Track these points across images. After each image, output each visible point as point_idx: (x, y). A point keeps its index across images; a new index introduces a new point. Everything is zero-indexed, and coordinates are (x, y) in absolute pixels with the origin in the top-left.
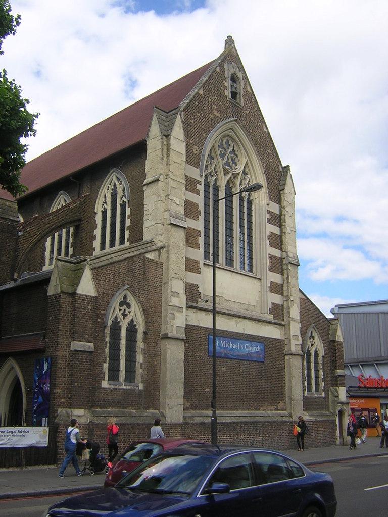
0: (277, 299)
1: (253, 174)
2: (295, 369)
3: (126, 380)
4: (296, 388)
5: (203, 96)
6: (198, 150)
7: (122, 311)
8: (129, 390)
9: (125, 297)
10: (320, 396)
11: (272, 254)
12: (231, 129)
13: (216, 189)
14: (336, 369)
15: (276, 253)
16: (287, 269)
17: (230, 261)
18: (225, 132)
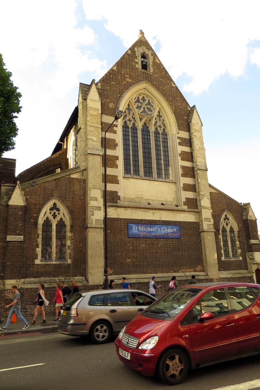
0: (190, 195)
2: (209, 240)
4: (211, 256)
5: (117, 71)
6: (113, 105)
8: (58, 264)
9: (226, 215)
10: (238, 259)
11: (183, 165)
12: (145, 89)
13: (134, 128)
14: (250, 240)
16: (197, 173)
17: (137, 172)
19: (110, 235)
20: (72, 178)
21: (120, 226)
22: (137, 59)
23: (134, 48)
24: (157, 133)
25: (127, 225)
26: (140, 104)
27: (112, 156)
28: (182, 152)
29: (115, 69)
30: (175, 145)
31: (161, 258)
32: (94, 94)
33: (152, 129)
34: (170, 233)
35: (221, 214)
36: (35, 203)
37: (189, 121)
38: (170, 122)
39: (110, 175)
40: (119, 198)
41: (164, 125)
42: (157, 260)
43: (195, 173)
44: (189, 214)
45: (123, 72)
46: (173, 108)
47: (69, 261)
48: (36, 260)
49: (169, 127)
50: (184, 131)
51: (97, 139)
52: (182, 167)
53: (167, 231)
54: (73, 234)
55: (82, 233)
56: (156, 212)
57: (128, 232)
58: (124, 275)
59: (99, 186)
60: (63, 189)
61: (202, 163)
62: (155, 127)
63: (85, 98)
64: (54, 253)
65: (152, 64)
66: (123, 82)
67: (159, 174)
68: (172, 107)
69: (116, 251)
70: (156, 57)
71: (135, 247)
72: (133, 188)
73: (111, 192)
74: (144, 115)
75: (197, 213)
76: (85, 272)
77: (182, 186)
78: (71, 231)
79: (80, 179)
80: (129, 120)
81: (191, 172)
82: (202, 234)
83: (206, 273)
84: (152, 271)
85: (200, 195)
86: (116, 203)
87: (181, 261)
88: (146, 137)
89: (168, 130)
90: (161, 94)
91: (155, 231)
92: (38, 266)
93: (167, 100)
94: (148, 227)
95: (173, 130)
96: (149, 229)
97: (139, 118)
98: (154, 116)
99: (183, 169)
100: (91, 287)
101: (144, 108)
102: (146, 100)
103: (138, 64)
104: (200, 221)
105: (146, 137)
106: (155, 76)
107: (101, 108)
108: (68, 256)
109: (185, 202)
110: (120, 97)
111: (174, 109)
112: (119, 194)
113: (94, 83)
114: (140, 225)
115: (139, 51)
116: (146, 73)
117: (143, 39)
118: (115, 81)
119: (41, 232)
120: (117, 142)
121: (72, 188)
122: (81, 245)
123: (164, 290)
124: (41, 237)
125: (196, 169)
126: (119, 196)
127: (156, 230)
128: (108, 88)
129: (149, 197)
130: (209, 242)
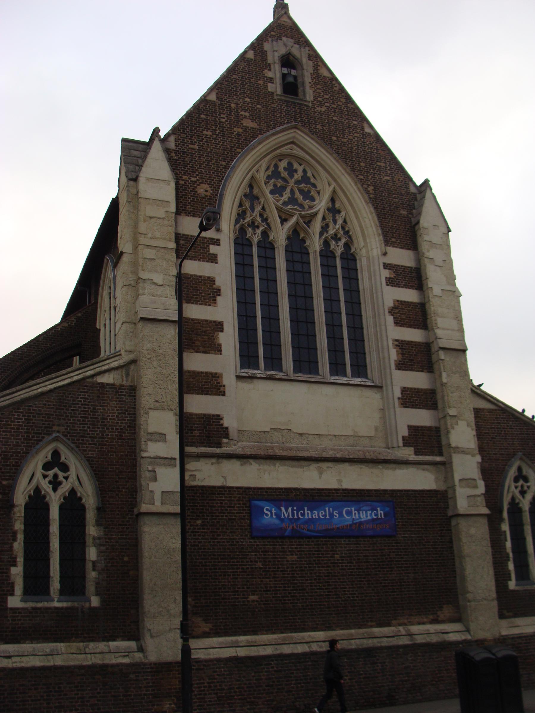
0: (423, 418)
1: (349, 208)
3: (62, 592)
6: (209, 189)
7: (519, 488)
8: (67, 608)
9: (520, 469)
13: (267, 246)
15: (414, 335)
17: (274, 361)
18: (278, 151)
19: (202, 532)
20: (99, 383)
21: (228, 507)
22: (270, 70)
23: (262, 44)
24: (327, 254)
25: (248, 505)
28: (396, 303)
29: (213, 97)
31: (341, 588)
32: (157, 166)
33: (315, 245)
34: (367, 522)
35: (507, 467)
36: (5, 452)
37: (414, 221)
38: (363, 224)
39: (202, 373)
40: (225, 432)
41: (347, 233)
42: (330, 595)
43: (434, 358)
44: (418, 468)
45: (233, 106)
46: (369, 189)
47: (95, 601)
48: (10, 598)
51: (164, 279)
52: (397, 343)
53: (357, 517)
54: (105, 531)
55: (128, 528)
56: (328, 467)
57: (251, 523)
58: (240, 635)
59: (169, 403)
60: (77, 412)
61: (453, 330)
62: (322, 241)
63: (134, 177)
64: (54, 579)
65: (310, 81)
66: (235, 129)
67: (337, 367)
68: (366, 186)
69: (218, 572)
70: (320, 63)
71: (270, 562)
72: (264, 406)
75: (439, 466)
76: (138, 629)
77: (398, 393)
78: (98, 523)
79: (122, 386)
81: (419, 356)
82: (453, 522)
83: (465, 626)
84: (317, 624)
85: (448, 418)
87: (397, 595)
88: (298, 267)
89: (359, 243)
90: (335, 155)
91: (325, 518)
92: (15, 613)
93: (353, 169)
94: (306, 508)
96: (308, 514)
98: (319, 211)
100: (151, 668)
103: (273, 83)
104: (448, 488)
105: (298, 267)
106: (319, 109)
108: (91, 587)
109: (406, 437)
111: (371, 192)
114: (283, 503)
115: (275, 51)
116: (294, 103)
117: (284, 21)
118: (214, 128)
119: (22, 527)
120: (218, 283)
121: (99, 409)
122: (126, 559)
123: (349, 672)
124: (23, 539)
125: (434, 348)
126: (227, 428)
127: (328, 517)
128: (196, 147)
129: (308, 424)
130: (474, 542)
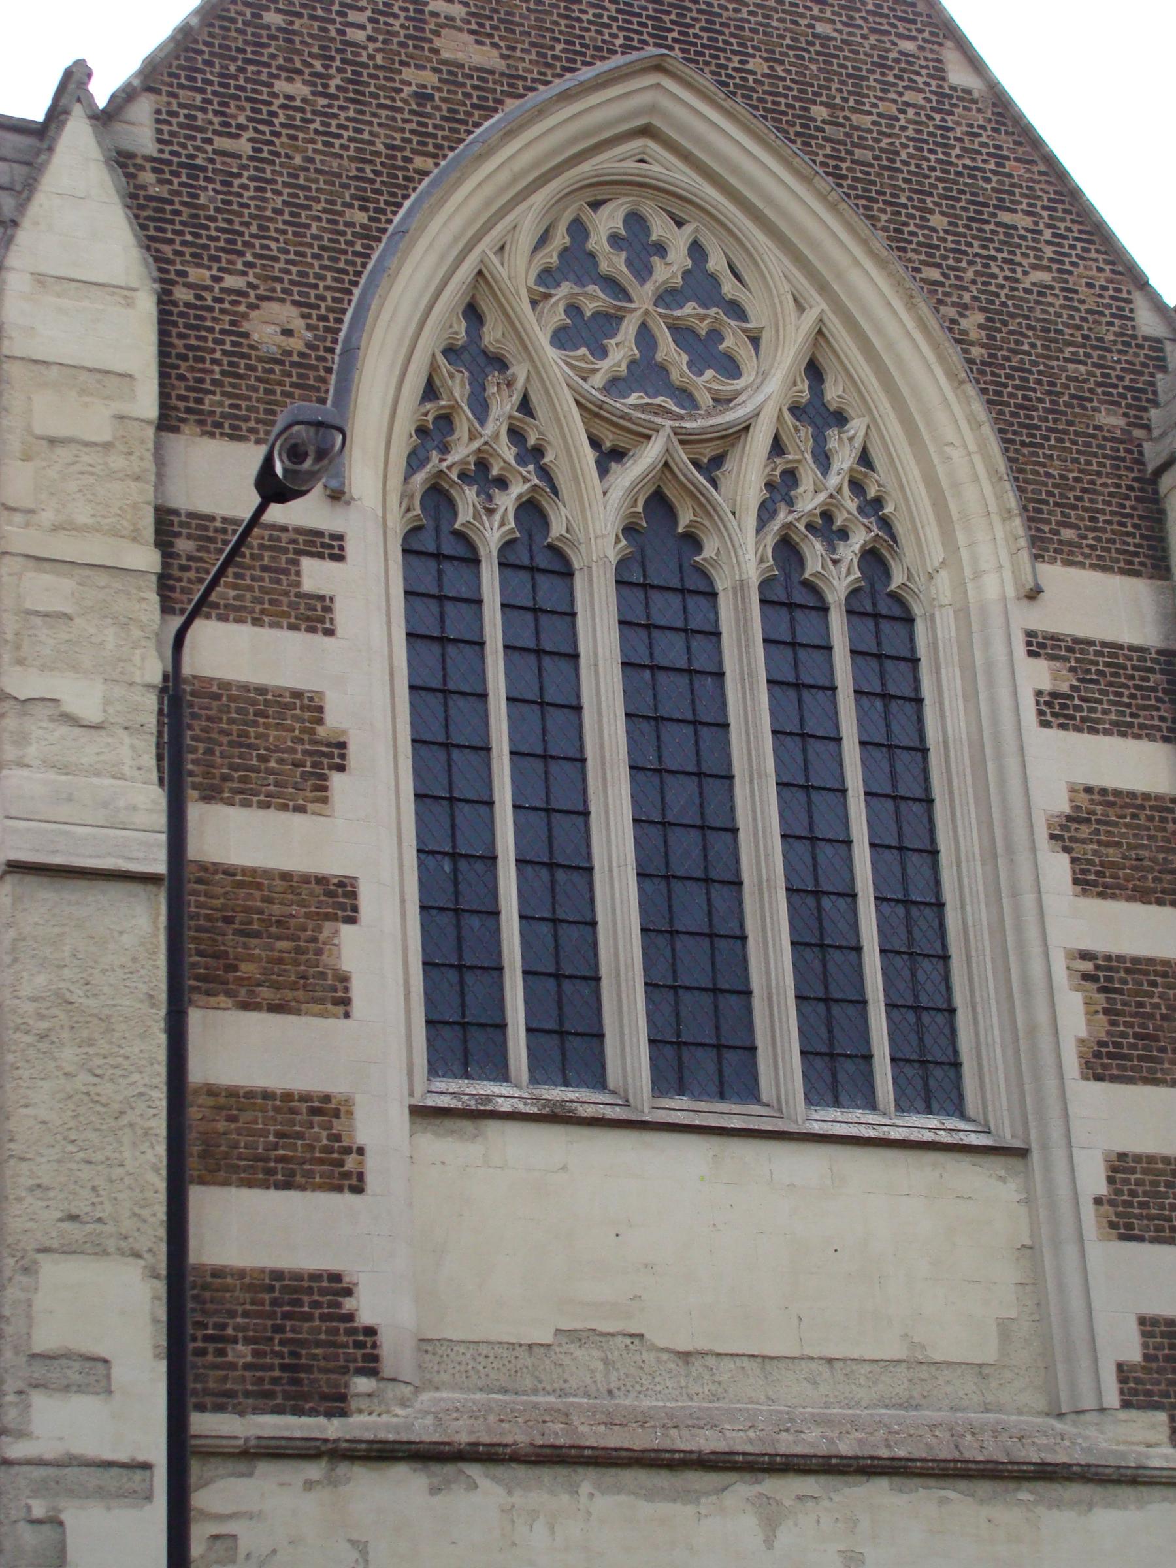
6: (298, 324)
13: (540, 563)
17: (569, 1043)
24: (790, 598)
26: (594, 300)
27: (286, 876)
30: (1007, 727)
33: (740, 557)
39: (267, 1095)
40: (363, 1349)
46: (964, 323)
49: (932, 533)
50: (1093, 567)
51: (107, 702)
52: (1088, 966)
62: (770, 540)
66: (408, 73)
67: (835, 1067)
68: (951, 312)
73: (271, 1289)
74: (643, 408)
80: (482, 475)
86: (329, 1414)
89: (921, 562)
90: (825, 184)
93: (898, 242)
95: (974, 559)
97: (595, 443)
99: (1102, 990)
101: (645, 335)
102: (661, 249)
105: (671, 650)
107: (162, 364)
109: (1133, 1367)
110: (370, 236)
111: (974, 335)
112: (367, 1307)
113: (85, 98)
118: (318, 66)
120: (335, 719)
126: (371, 1331)
128: (243, 146)
